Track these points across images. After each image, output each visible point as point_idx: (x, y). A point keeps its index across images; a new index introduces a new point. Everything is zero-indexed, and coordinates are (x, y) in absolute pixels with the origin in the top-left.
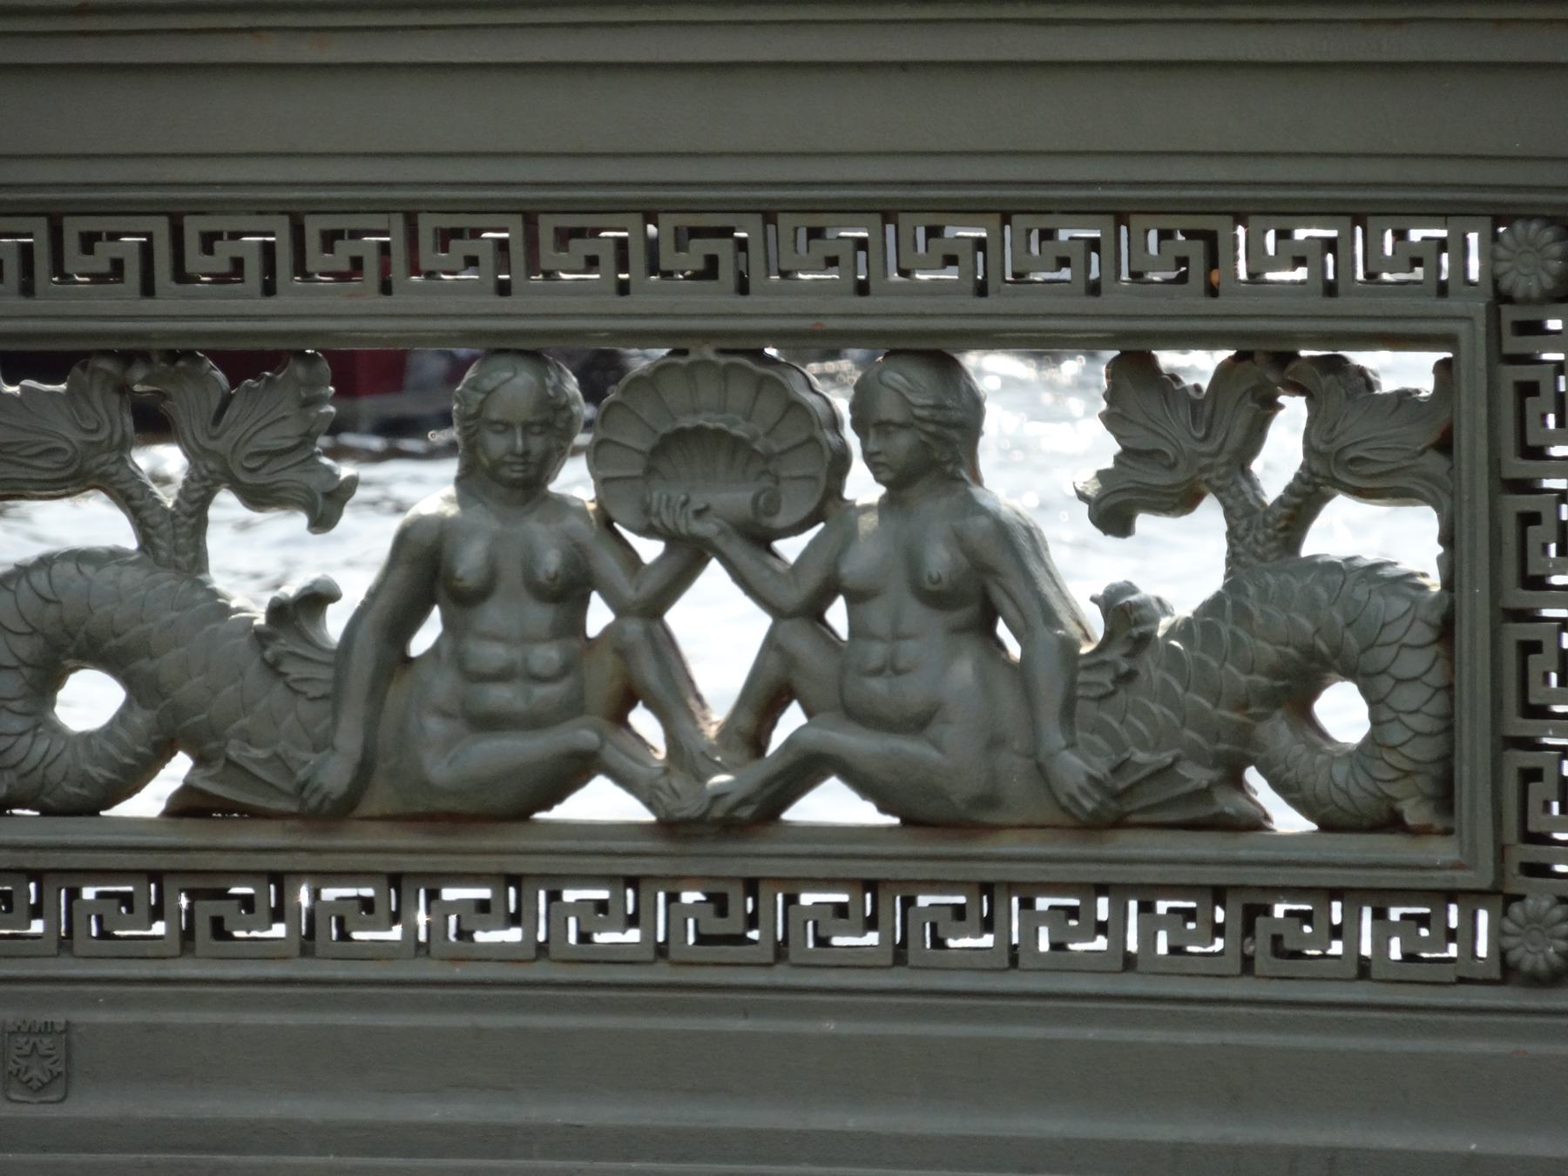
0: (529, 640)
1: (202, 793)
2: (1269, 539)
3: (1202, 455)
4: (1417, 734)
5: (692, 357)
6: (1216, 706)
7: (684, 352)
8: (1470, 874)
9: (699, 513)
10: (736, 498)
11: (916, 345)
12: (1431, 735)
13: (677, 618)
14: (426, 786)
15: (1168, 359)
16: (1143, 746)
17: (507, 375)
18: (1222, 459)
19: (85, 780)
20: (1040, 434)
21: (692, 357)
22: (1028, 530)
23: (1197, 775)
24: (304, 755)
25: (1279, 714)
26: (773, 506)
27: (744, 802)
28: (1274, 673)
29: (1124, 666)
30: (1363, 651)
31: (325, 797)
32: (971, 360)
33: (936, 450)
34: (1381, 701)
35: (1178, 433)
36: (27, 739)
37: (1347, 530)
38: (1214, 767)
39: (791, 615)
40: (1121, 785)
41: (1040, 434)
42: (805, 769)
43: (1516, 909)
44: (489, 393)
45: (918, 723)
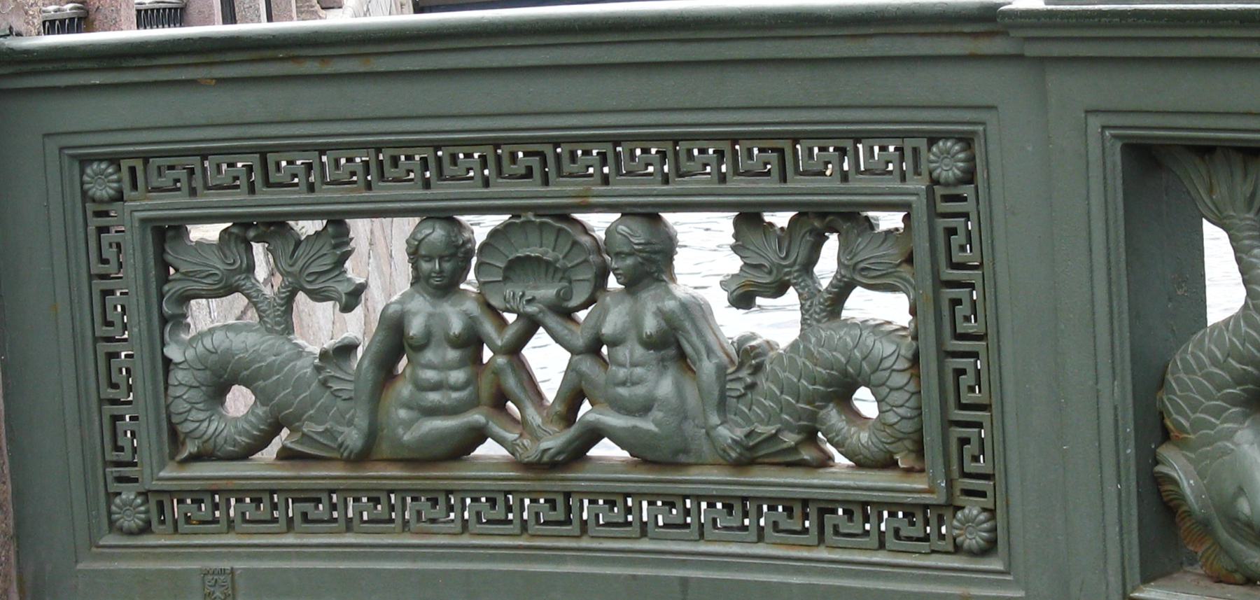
0: (452, 367)
1: (290, 449)
2: (822, 311)
3: (786, 266)
4: (903, 418)
5: (523, 219)
6: (798, 402)
7: (519, 217)
8: (935, 496)
9: (529, 302)
10: (548, 292)
11: (639, 210)
12: (910, 418)
13: (527, 352)
14: (402, 445)
15: (768, 217)
16: (761, 422)
17: (428, 232)
18: (796, 268)
19: (235, 443)
20: (704, 250)
21: (523, 219)
22: (700, 305)
23: (790, 439)
24: (340, 429)
25: (831, 405)
26: (568, 296)
27: (558, 453)
28: (827, 384)
29: (749, 380)
30: (874, 372)
31: (351, 452)
32: (669, 217)
33: (654, 263)
34: (883, 400)
35: (771, 254)
36: (206, 424)
37: (865, 305)
38: (799, 433)
39: (578, 354)
40: (751, 444)
41: (704, 250)
42: (594, 434)
43: (959, 514)
44: (420, 241)
45: (644, 408)
